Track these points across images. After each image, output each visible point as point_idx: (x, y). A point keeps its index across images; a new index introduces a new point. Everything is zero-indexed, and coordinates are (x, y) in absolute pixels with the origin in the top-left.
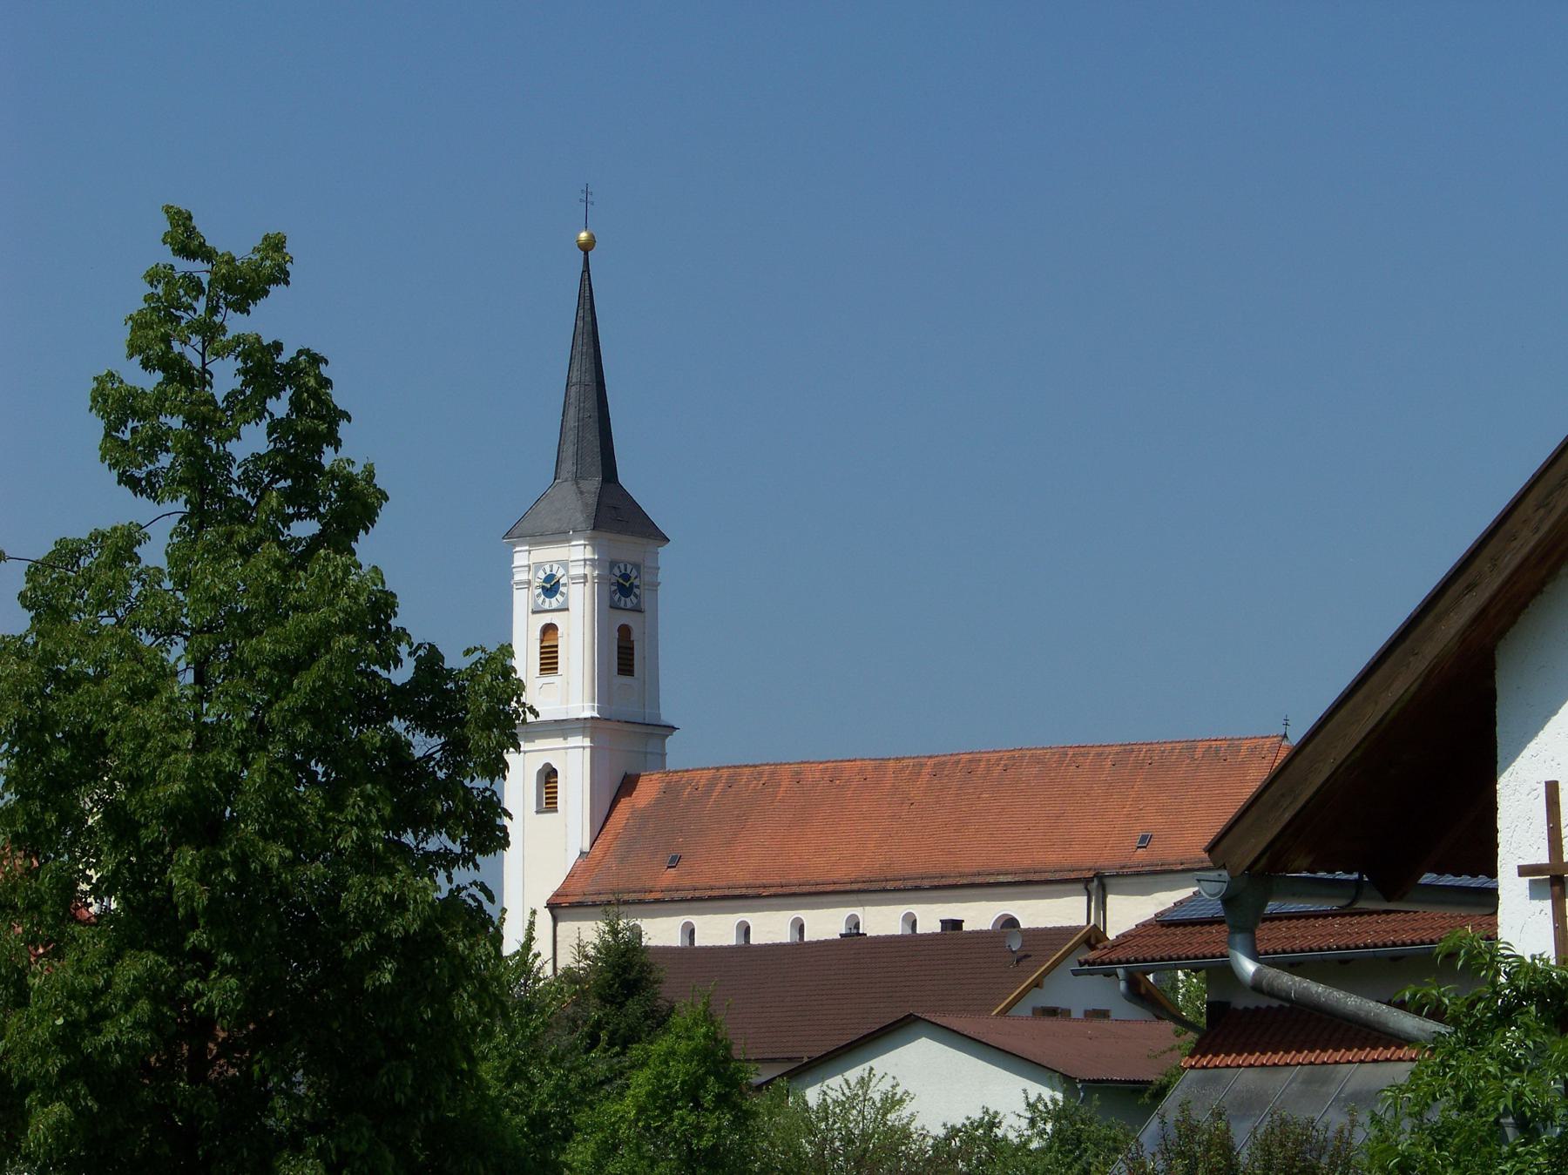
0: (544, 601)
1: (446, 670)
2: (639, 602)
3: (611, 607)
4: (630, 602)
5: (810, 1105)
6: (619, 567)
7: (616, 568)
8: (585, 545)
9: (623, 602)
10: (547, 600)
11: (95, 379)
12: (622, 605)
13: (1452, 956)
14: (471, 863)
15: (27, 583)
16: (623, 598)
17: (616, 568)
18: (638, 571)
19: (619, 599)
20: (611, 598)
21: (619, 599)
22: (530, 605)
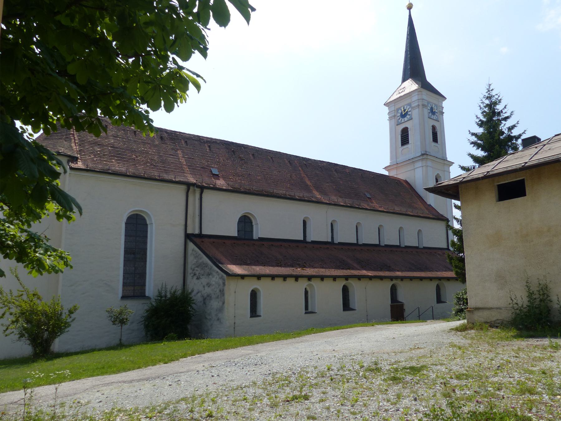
0: (402, 120)
1: (35, 350)
2: (438, 118)
3: (429, 118)
4: (434, 117)
5: (512, 131)
6: (430, 104)
7: (429, 104)
8: (418, 94)
9: (434, 117)
10: (401, 118)
11: (525, 133)
12: (432, 118)
13: (471, 168)
14: (455, 276)
15: (385, 168)
16: (432, 116)
17: (429, 104)
18: (437, 107)
19: (431, 116)
20: (429, 115)
21: (431, 116)
22: (396, 123)
